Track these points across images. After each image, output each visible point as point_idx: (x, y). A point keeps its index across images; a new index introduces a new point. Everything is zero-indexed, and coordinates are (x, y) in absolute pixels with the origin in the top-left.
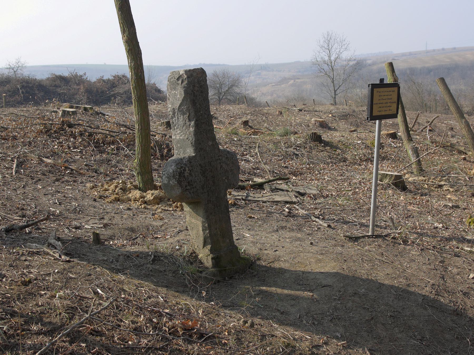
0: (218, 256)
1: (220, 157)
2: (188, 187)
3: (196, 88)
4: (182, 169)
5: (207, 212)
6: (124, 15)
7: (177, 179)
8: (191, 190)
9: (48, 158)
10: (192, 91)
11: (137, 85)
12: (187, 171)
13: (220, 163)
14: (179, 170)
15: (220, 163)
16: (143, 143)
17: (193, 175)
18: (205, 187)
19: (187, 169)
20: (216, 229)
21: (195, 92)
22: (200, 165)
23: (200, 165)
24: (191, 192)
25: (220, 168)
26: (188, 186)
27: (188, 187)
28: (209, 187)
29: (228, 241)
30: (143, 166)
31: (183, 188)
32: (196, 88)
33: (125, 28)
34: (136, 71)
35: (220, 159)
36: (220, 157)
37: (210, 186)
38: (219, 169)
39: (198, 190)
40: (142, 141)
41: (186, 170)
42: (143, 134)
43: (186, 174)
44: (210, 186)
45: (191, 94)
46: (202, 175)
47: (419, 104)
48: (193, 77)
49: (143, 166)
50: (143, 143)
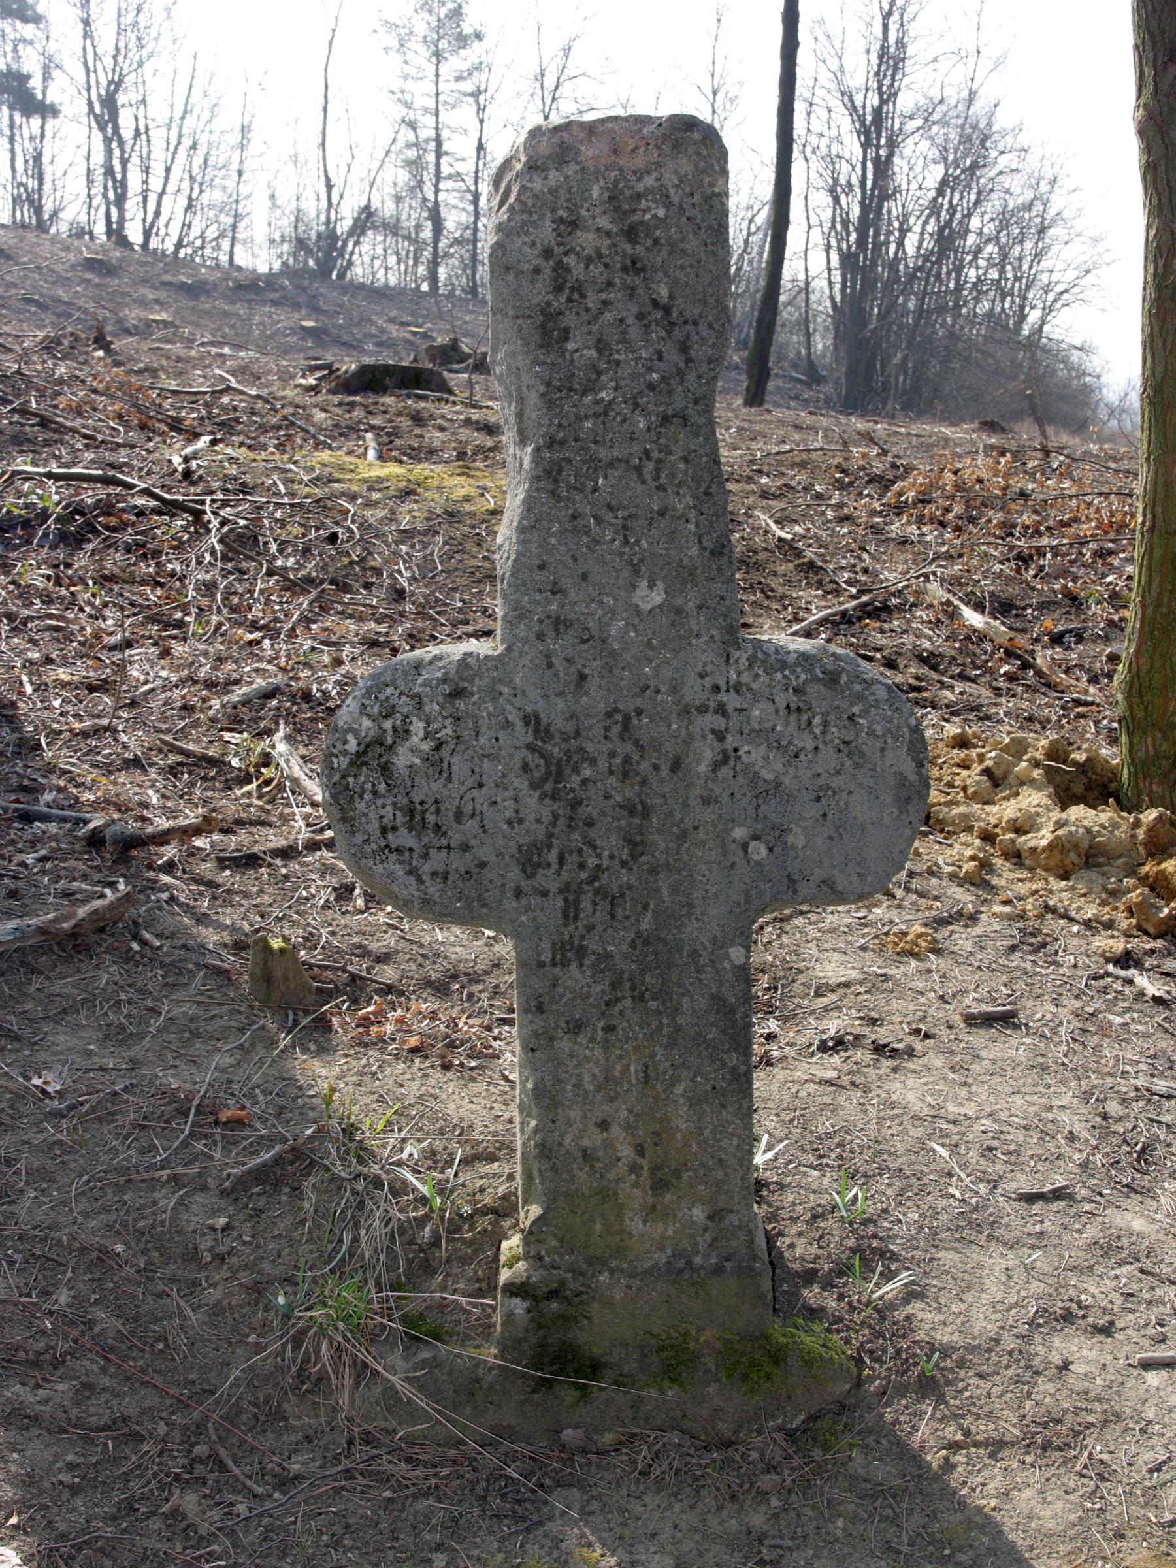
0: (562, 1283)
1: (723, 697)
2: (403, 839)
3: (586, 240)
4: (388, 725)
5: (540, 1009)
6: (1150, 8)
7: (337, 777)
8: (425, 856)
9: (979, 607)
10: (547, 253)
11: (1156, 329)
12: (415, 740)
13: (720, 736)
14: (366, 723)
15: (720, 736)
16: (1154, 593)
17: (459, 766)
18: (553, 857)
19: (418, 727)
20: (604, 1125)
21: (570, 260)
22: (531, 720)
23: (531, 720)
24: (426, 868)
25: (716, 766)
26: (403, 831)
27: (403, 839)
28: (582, 866)
29: (699, 1214)
30: (1141, 695)
31: (358, 838)
32: (586, 240)
33: (1146, 70)
34: (1161, 263)
35: (721, 709)
36: (732, 701)
37: (592, 862)
38: (702, 769)
39: (483, 865)
40: (1149, 583)
41: (407, 732)
42: (1158, 553)
43: (403, 759)
44: (592, 862)
45: (537, 271)
46: (534, 786)
47: (847, 95)
48: (570, 170)
49: (1141, 695)
50: (1154, 593)
